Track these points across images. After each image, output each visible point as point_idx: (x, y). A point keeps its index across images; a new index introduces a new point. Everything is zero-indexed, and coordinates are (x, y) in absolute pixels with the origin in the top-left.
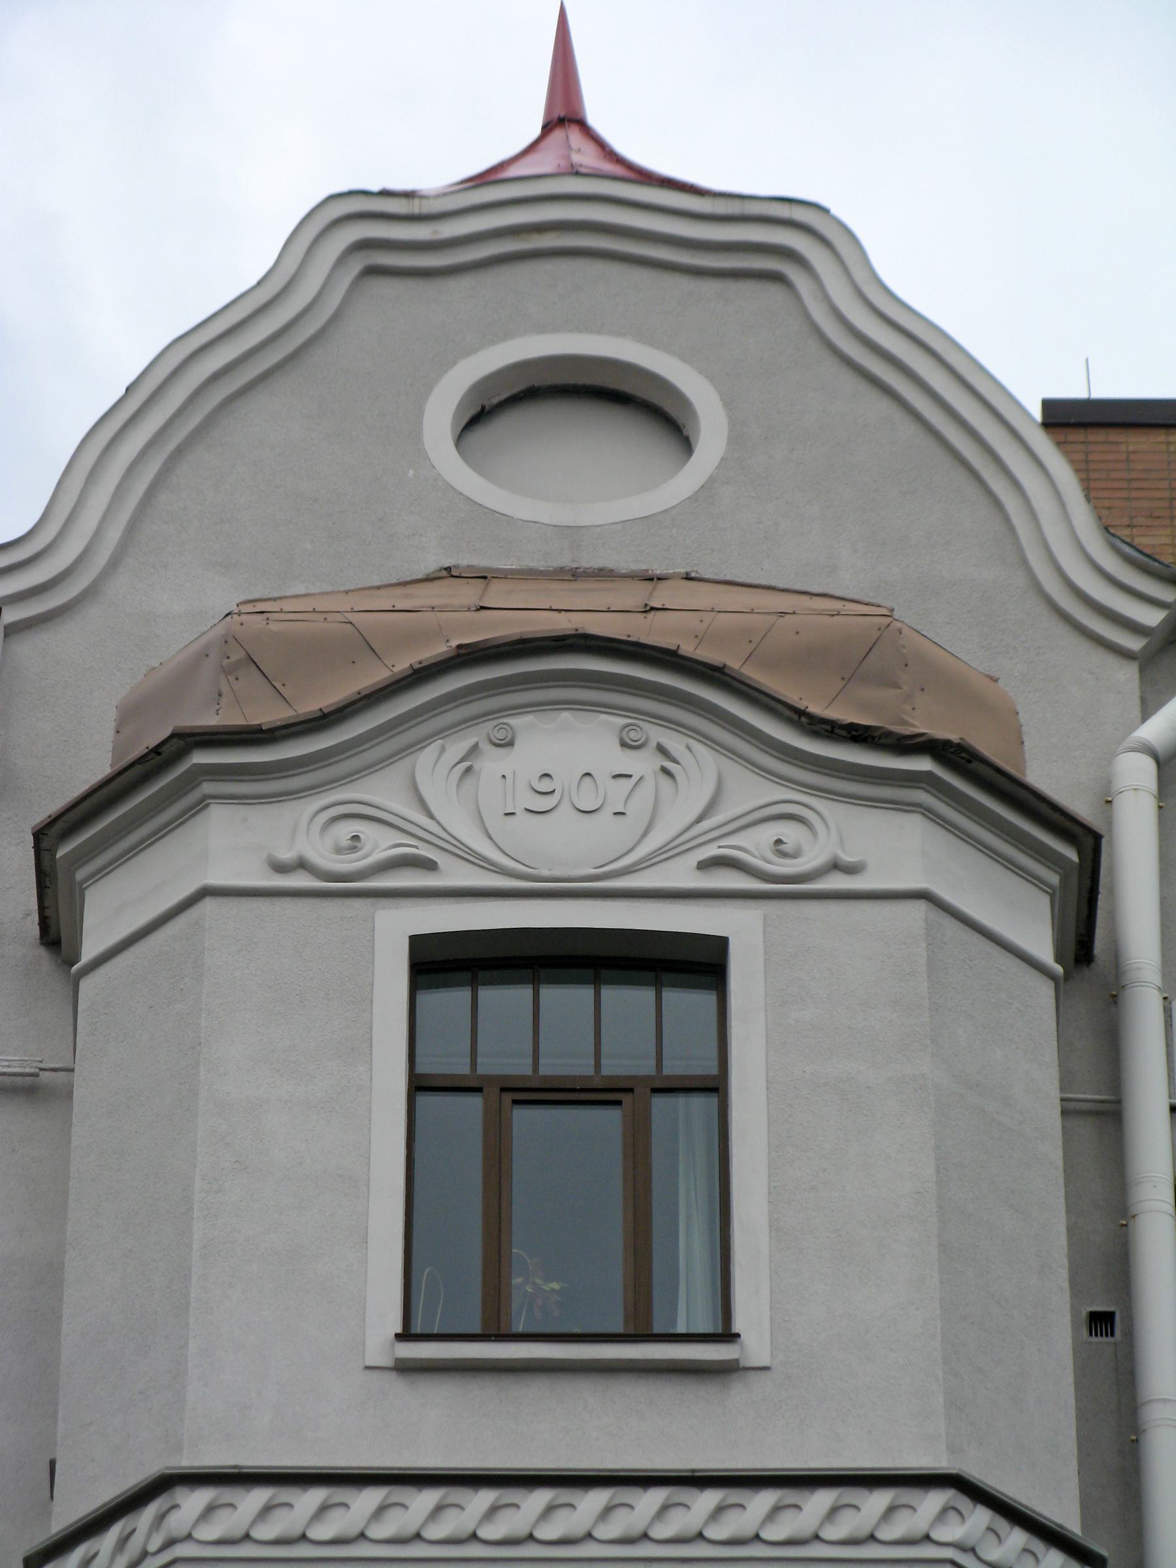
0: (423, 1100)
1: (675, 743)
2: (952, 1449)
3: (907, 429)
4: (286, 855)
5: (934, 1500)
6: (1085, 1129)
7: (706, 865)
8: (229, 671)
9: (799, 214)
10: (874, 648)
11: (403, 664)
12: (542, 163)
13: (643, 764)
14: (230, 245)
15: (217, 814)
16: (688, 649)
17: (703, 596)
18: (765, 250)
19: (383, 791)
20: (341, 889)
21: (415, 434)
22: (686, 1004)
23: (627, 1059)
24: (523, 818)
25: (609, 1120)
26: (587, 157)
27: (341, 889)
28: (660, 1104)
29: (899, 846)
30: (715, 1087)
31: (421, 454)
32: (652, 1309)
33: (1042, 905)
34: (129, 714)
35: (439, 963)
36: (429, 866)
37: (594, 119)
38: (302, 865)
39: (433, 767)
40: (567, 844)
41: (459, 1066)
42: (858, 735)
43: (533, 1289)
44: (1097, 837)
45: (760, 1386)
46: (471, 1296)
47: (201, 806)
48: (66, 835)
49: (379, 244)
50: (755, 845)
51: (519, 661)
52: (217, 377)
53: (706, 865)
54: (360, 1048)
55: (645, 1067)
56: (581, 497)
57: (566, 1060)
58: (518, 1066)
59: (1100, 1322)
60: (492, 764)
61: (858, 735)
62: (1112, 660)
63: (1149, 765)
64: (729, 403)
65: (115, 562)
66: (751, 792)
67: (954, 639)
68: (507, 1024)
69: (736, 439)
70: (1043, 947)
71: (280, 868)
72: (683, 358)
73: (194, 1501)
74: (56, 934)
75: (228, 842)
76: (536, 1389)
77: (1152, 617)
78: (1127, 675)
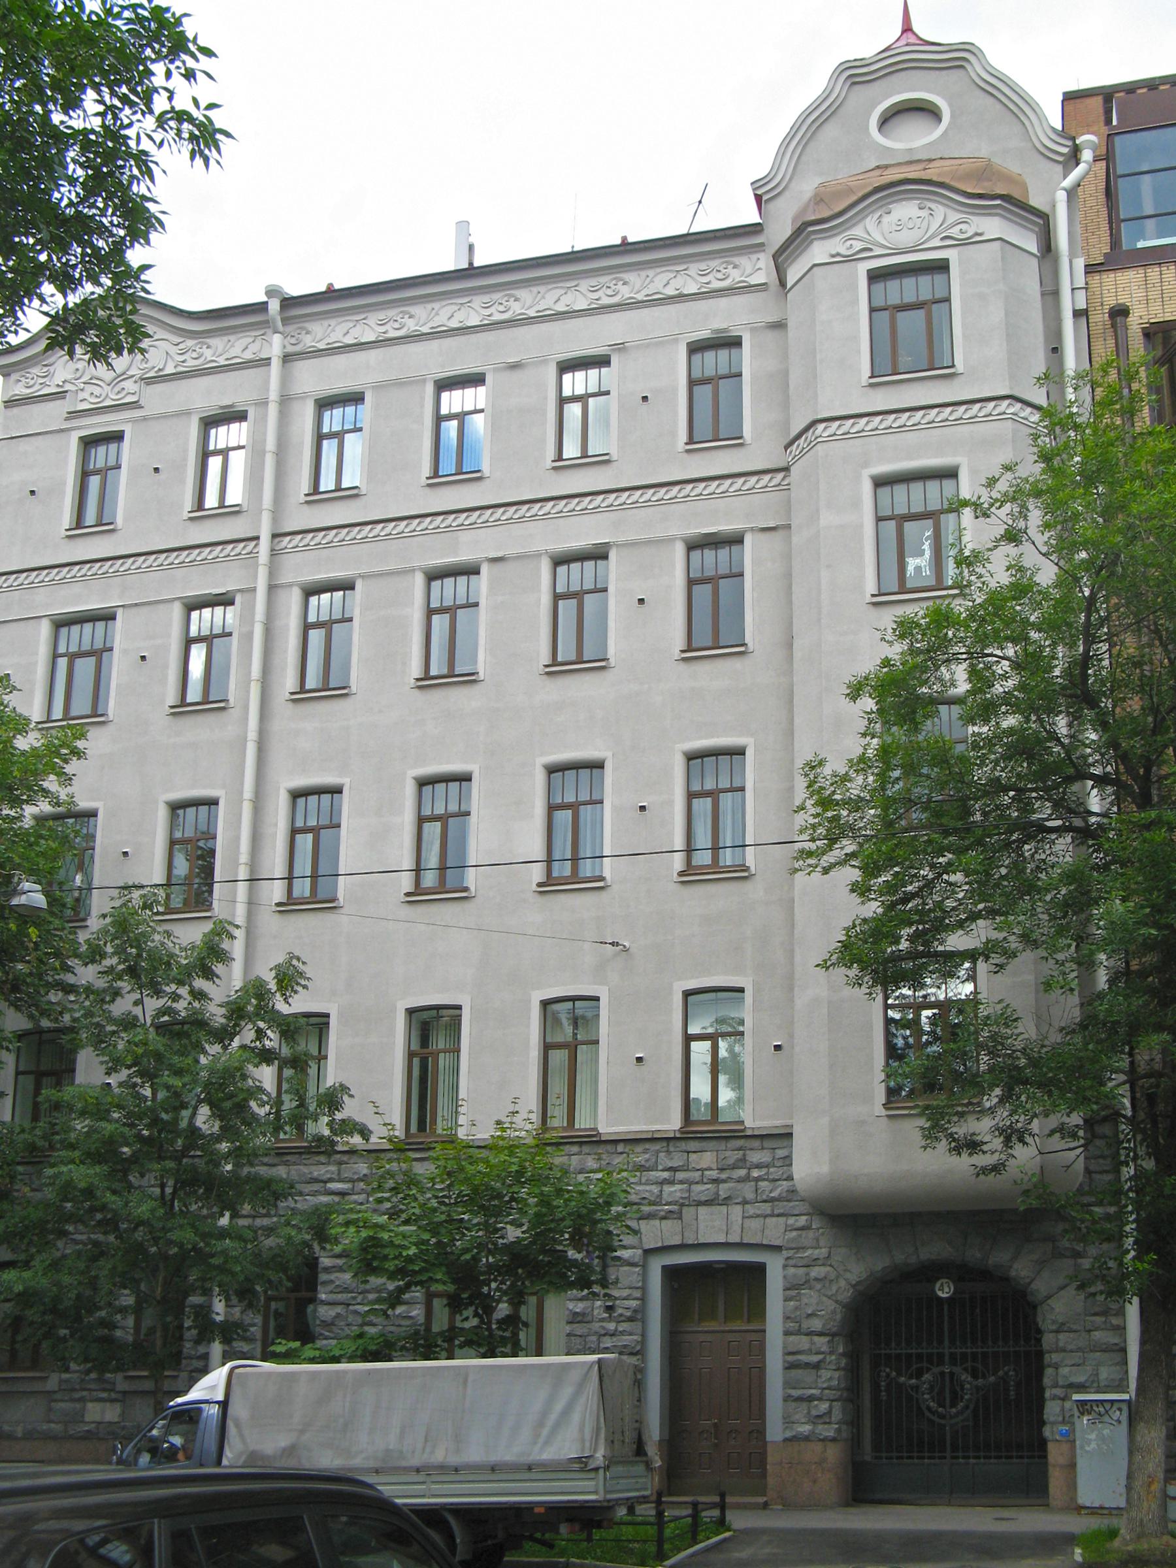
0: (874, 314)
1: (933, 206)
2: (1011, 388)
3: (999, 106)
4: (834, 252)
5: (1006, 402)
6: (1049, 298)
7: (942, 239)
8: (817, 203)
9: (967, 47)
10: (986, 171)
11: (860, 194)
12: (903, 42)
13: (924, 213)
14: (814, 84)
15: (816, 243)
16: (935, 179)
17: (942, 163)
18: (958, 59)
19: (858, 231)
20: (850, 259)
21: (867, 129)
22: (939, 278)
23: (925, 295)
24: (894, 234)
25: (921, 313)
26: (913, 40)
27: (850, 259)
28: (935, 306)
29: (992, 226)
30: (947, 300)
31: (869, 134)
32: (935, 362)
33: (1034, 237)
34: (794, 220)
35: (874, 276)
36: (870, 250)
37: (915, 29)
38: (838, 254)
39: (870, 222)
40: (906, 238)
41: (883, 304)
42: (980, 196)
43: (905, 360)
44: (1048, 216)
45: (962, 378)
46: (888, 365)
47: (811, 242)
48: (781, 255)
49: (855, 75)
50: (954, 232)
51: (890, 189)
52: (814, 121)
53: (942, 239)
54: (855, 302)
55: (929, 297)
56: (915, 138)
57: (909, 298)
58: (897, 301)
59: (1055, 350)
60: (886, 219)
61: (980, 196)
62: (1051, 164)
63: (1064, 193)
64: (950, 105)
65: (790, 180)
66: (954, 216)
67: (1013, 167)
68: (895, 292)
69: (953, 116)
70: (1034, 249)
71: (833, 256)
72: (938, 95)
73: (821, 426)
74: (782, 283)
75: (819, 251)
76: (904, 387)
77: (1065, 150)
78: (1059, 169)
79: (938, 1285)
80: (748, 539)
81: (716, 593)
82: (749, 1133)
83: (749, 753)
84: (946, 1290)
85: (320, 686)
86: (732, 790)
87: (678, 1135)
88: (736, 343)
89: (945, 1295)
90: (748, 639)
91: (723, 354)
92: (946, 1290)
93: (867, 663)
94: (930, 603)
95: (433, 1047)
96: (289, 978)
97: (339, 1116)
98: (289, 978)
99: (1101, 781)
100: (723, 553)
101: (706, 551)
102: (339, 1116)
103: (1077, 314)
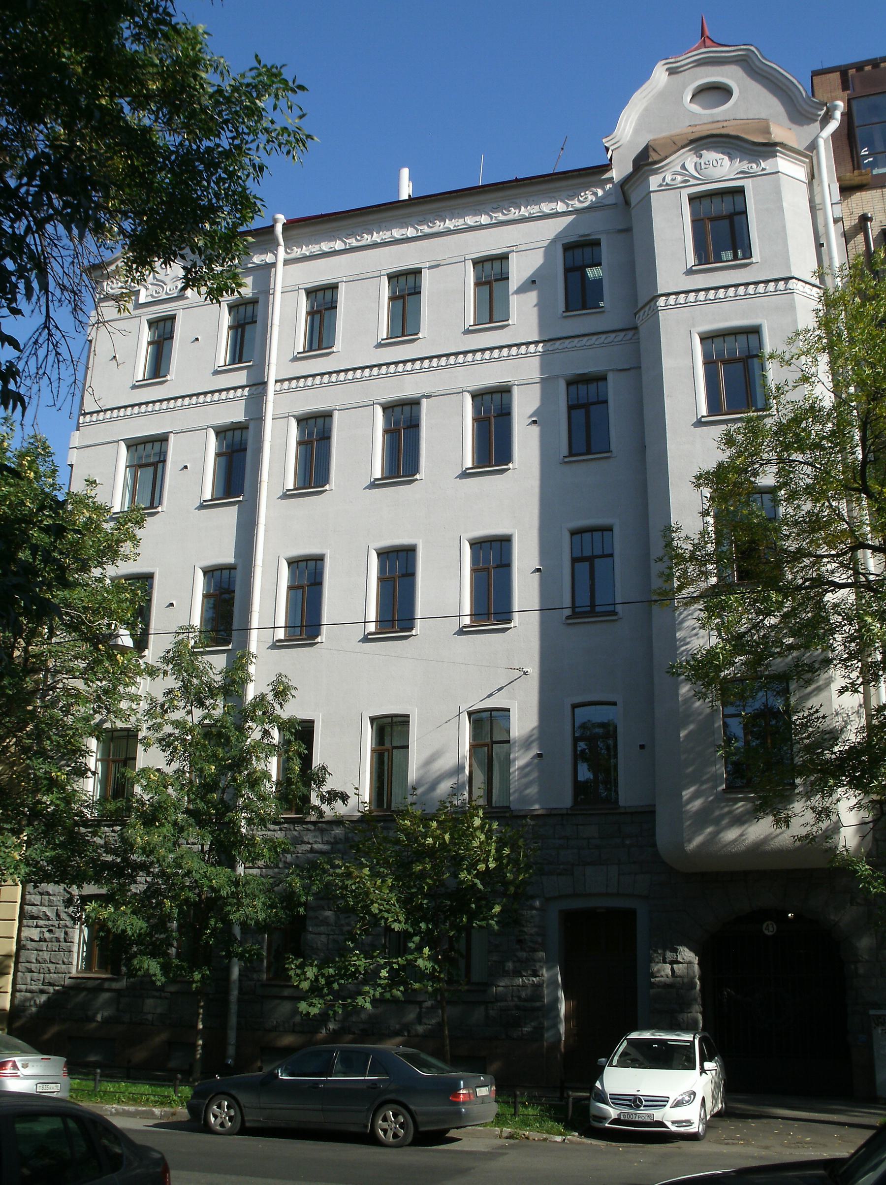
79: (765, 925)
80: (610, 377)
81: (491, 738)
82: (623, 810)
83: (616, 530)
84: (771, 929)
85: (388, 475)
86: (604, 556)
87: (569, 812)
88: (597, 243)
89: (770, 934)
90: (613, 447)
91: (587, 250)
92: (771, 929)
93: (710, 465)
94: (724, 427)
95: (387, 745)
96: (282, 692)
97: (325, 789)
98: (282, 692)
99: (875, 549)
100: (592, 387)
101: (580, 386)
102: (325, 789)
103: (836, 221)
